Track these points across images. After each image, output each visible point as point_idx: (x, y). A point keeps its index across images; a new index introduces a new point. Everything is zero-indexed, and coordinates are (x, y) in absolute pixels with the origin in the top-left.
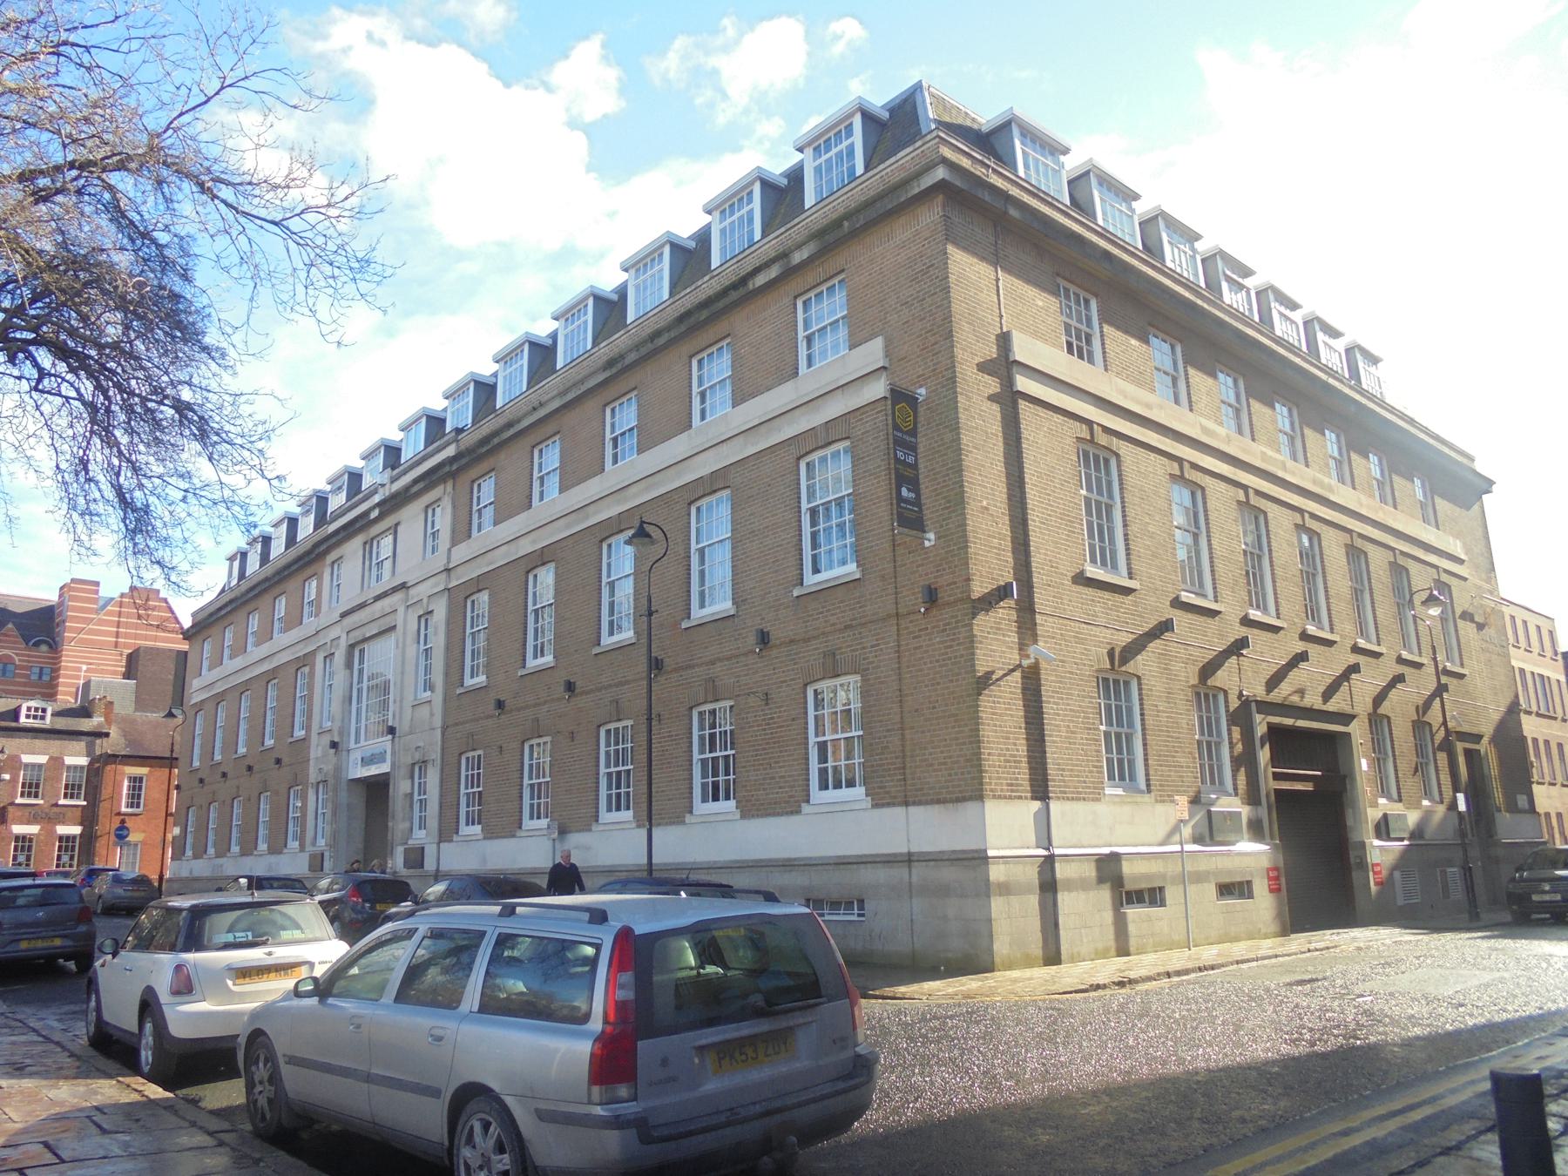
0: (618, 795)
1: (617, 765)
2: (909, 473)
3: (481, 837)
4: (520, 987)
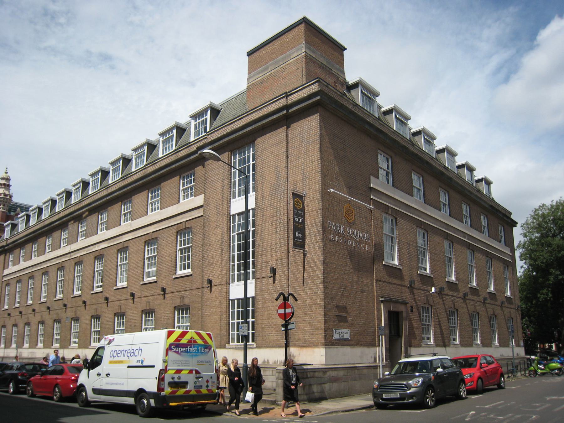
0: (120, 322)
2: (300, 226)
3: (77, 348)
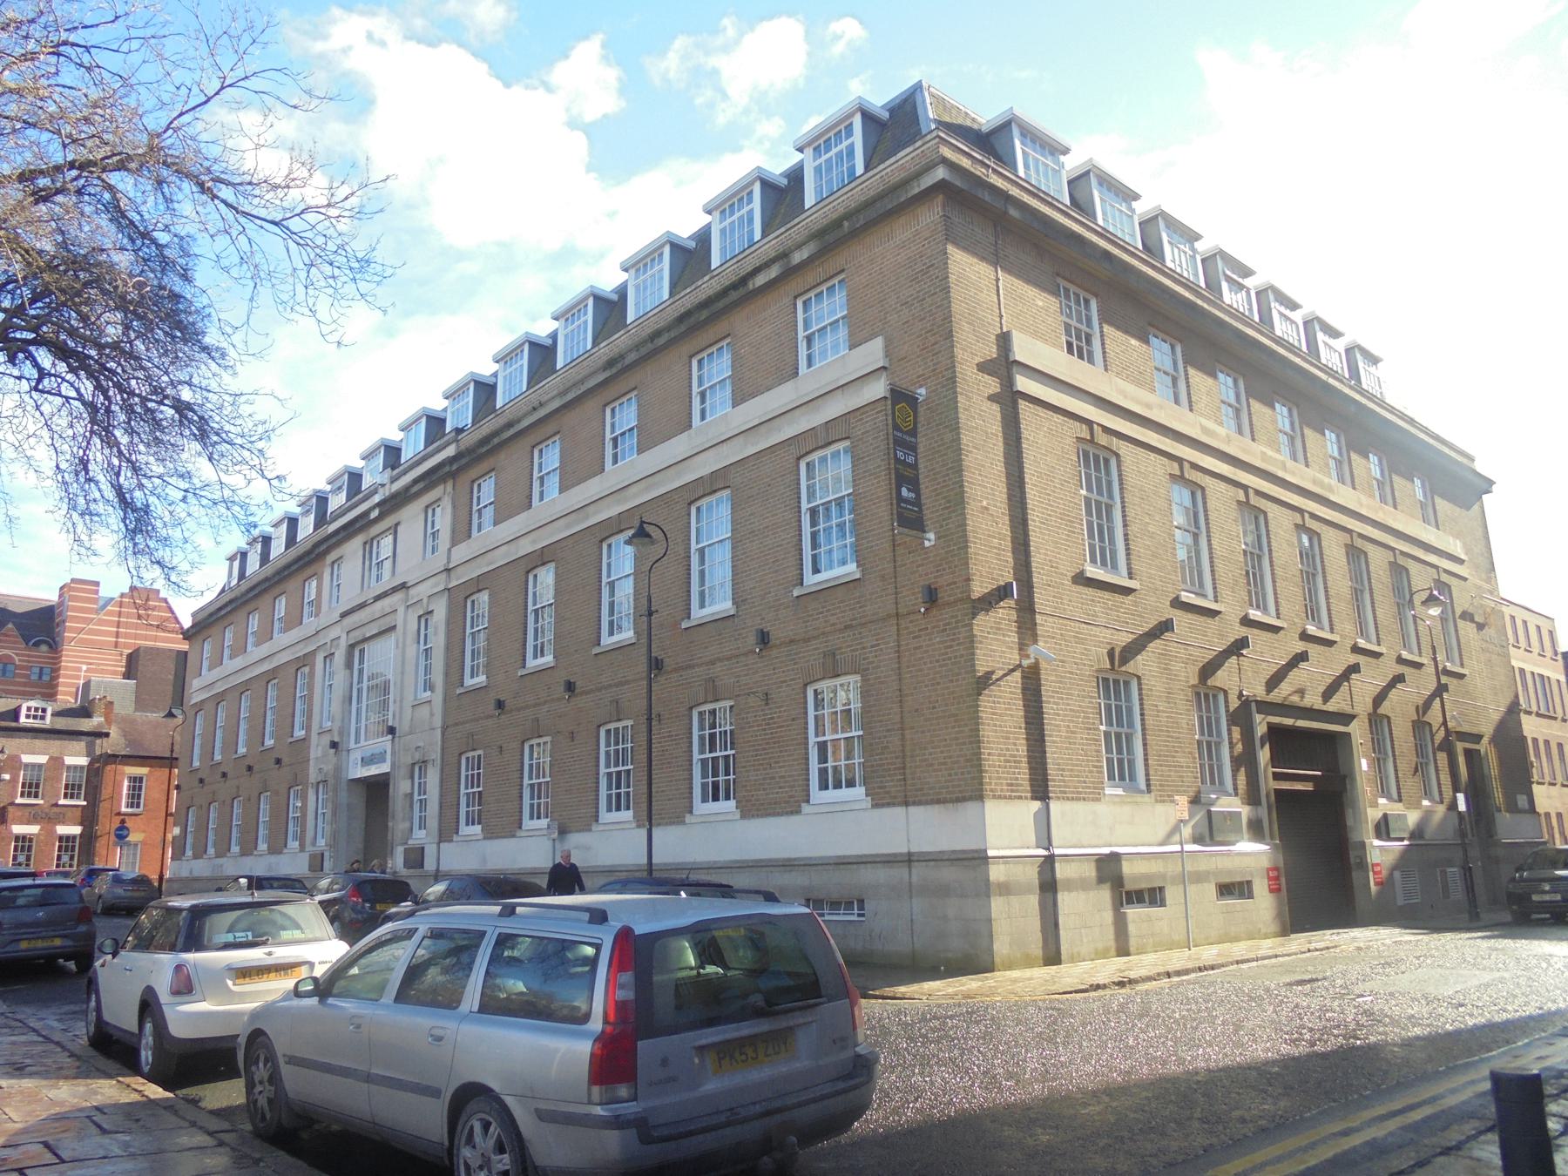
0: (618, 795)
1: (617, 765)
2: (909, 473)
3: (481, 837)
4: (520, 987)
